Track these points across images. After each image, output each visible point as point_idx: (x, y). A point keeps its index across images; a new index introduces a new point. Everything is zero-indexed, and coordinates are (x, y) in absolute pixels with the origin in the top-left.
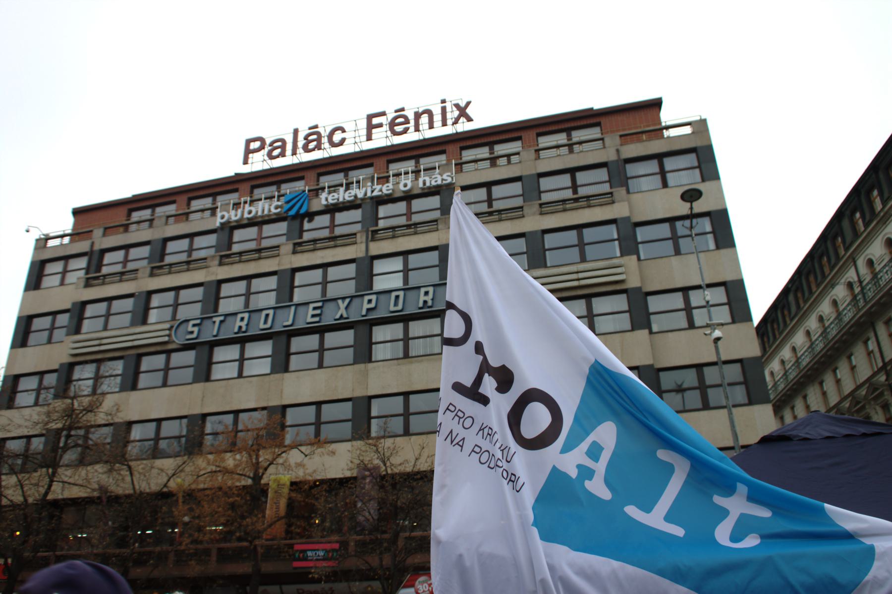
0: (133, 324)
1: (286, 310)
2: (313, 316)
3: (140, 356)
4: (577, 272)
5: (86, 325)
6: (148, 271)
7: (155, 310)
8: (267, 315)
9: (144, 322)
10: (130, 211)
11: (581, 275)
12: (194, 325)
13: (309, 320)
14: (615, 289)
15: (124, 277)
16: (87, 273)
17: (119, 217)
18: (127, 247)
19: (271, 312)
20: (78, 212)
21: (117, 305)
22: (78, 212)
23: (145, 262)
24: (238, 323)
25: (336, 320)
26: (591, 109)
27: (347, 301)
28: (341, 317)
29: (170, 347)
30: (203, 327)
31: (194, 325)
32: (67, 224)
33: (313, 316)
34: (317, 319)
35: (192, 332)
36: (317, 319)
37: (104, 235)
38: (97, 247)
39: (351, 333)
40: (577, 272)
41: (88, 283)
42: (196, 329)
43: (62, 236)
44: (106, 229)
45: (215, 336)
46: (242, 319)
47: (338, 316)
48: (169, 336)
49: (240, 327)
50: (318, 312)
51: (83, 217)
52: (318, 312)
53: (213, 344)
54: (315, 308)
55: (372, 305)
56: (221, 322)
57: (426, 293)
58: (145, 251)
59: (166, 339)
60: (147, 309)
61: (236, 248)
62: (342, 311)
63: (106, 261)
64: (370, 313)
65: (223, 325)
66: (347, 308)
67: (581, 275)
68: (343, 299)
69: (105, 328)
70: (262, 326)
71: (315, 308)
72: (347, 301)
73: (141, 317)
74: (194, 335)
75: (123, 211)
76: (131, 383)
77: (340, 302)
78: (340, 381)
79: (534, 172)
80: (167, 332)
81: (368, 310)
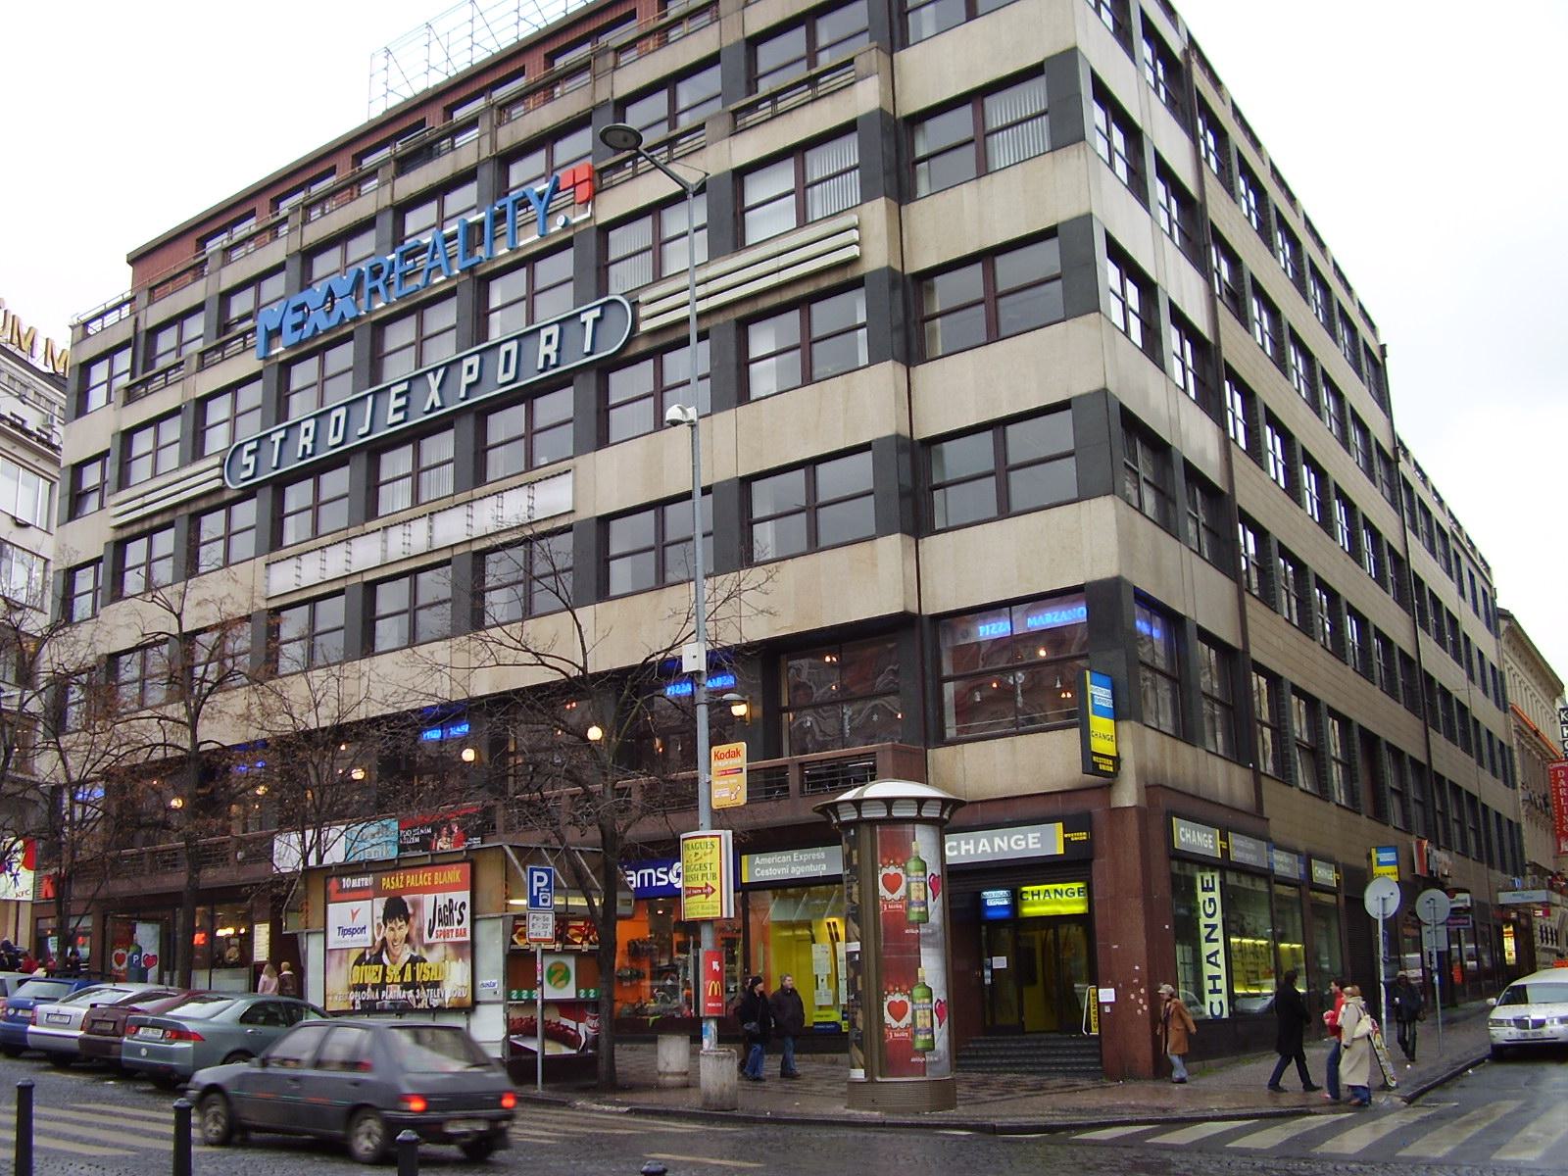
0: (715, 253)
1: (361, 404)
2: (397, 411)
3: (743, 325)
4: (142, 496)
5: (758, 226)
6: (725, 124)
7: (498, 313)
8: (508, 354)
9: (739, 244)
10: (202, 242)
11: (148, 498)
12: (250, 453)
13: (392, 418)
14: (842, 280)
15: (781, 106)
16: (132, 378)
17: (186, 254)
18: (669, 83)
19: (513, 346)
20: (136, 259)
21: (820, 163)
22: (136, 259)
23: (716, 106)
24: (544, 349)
25: (427, 413)
26: (427, 90)
27: (441, 372)
28: (433, 408)
29: (227, 496)
30: (262, 454)
31: (250, 453)
32: (121, 281)
33: (397, 411)
34: (400, 416)
35: (247, 466)
36: (400, 416)
37: (151, 302)
38: (142, 327)
39: (568, 393)
40: (142, 496)
41: (131, 395)
42: (252, 459)
43: (118, 307)
44: (152, 289)
45: (589, 354)
46: (549, 339)
47: (427, 408)
48: (222, 477)
49: (547, 357)
50: (402, 401)
51: (146, 265)
52: (402, 401)
53: (482, 412)
54: (399, 396)
55: (474, 377)
56: (596, 321)
57: (549, 339)
58: (710, 81)
59: (217, 483)
60: (740, 212)
61: (765, 87)
62: (434, 397)
63: (763, 66)
64: (473, 391)
65: (603, 327)
66: (440, 388)
67: (148, 498)
68: (435, 370)
69: (803, 221)
70: (502, 378)
71: (399, 396)
72: (441, 372)
73: (729, 231)
74: (249, 473)
75: (190, 243)
76: (474, 474)
77: (430, 376)
78: (864, 403)
79: (739, 36)
80: (217, 472)
81: (469, 386)
